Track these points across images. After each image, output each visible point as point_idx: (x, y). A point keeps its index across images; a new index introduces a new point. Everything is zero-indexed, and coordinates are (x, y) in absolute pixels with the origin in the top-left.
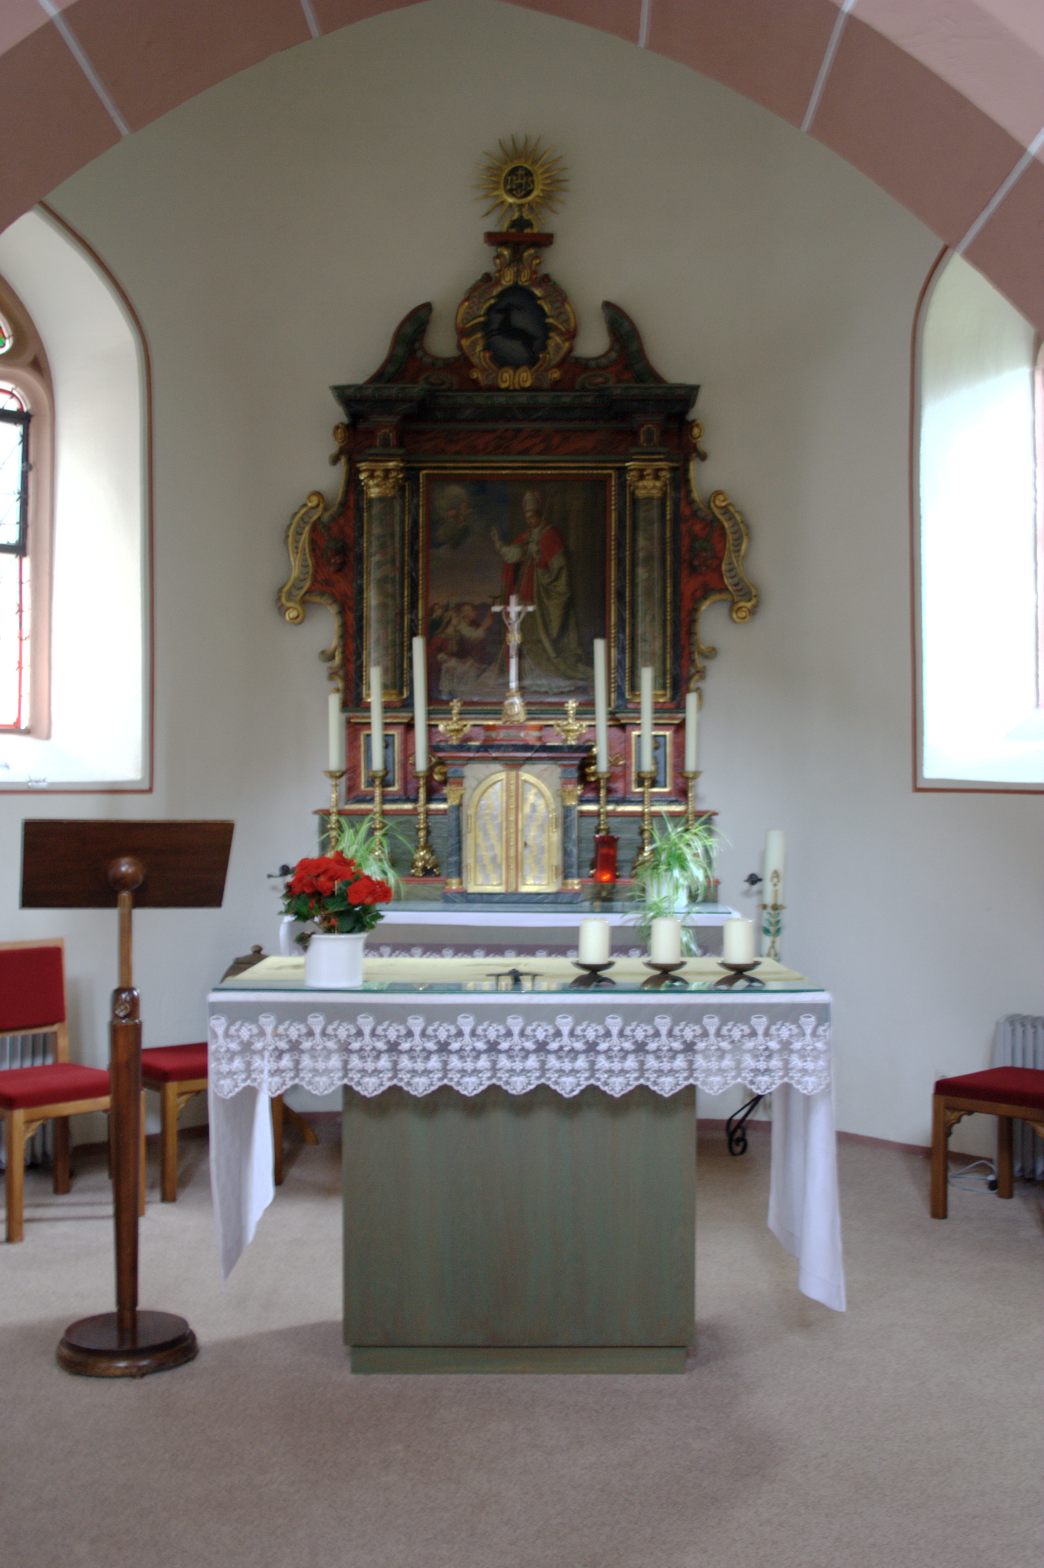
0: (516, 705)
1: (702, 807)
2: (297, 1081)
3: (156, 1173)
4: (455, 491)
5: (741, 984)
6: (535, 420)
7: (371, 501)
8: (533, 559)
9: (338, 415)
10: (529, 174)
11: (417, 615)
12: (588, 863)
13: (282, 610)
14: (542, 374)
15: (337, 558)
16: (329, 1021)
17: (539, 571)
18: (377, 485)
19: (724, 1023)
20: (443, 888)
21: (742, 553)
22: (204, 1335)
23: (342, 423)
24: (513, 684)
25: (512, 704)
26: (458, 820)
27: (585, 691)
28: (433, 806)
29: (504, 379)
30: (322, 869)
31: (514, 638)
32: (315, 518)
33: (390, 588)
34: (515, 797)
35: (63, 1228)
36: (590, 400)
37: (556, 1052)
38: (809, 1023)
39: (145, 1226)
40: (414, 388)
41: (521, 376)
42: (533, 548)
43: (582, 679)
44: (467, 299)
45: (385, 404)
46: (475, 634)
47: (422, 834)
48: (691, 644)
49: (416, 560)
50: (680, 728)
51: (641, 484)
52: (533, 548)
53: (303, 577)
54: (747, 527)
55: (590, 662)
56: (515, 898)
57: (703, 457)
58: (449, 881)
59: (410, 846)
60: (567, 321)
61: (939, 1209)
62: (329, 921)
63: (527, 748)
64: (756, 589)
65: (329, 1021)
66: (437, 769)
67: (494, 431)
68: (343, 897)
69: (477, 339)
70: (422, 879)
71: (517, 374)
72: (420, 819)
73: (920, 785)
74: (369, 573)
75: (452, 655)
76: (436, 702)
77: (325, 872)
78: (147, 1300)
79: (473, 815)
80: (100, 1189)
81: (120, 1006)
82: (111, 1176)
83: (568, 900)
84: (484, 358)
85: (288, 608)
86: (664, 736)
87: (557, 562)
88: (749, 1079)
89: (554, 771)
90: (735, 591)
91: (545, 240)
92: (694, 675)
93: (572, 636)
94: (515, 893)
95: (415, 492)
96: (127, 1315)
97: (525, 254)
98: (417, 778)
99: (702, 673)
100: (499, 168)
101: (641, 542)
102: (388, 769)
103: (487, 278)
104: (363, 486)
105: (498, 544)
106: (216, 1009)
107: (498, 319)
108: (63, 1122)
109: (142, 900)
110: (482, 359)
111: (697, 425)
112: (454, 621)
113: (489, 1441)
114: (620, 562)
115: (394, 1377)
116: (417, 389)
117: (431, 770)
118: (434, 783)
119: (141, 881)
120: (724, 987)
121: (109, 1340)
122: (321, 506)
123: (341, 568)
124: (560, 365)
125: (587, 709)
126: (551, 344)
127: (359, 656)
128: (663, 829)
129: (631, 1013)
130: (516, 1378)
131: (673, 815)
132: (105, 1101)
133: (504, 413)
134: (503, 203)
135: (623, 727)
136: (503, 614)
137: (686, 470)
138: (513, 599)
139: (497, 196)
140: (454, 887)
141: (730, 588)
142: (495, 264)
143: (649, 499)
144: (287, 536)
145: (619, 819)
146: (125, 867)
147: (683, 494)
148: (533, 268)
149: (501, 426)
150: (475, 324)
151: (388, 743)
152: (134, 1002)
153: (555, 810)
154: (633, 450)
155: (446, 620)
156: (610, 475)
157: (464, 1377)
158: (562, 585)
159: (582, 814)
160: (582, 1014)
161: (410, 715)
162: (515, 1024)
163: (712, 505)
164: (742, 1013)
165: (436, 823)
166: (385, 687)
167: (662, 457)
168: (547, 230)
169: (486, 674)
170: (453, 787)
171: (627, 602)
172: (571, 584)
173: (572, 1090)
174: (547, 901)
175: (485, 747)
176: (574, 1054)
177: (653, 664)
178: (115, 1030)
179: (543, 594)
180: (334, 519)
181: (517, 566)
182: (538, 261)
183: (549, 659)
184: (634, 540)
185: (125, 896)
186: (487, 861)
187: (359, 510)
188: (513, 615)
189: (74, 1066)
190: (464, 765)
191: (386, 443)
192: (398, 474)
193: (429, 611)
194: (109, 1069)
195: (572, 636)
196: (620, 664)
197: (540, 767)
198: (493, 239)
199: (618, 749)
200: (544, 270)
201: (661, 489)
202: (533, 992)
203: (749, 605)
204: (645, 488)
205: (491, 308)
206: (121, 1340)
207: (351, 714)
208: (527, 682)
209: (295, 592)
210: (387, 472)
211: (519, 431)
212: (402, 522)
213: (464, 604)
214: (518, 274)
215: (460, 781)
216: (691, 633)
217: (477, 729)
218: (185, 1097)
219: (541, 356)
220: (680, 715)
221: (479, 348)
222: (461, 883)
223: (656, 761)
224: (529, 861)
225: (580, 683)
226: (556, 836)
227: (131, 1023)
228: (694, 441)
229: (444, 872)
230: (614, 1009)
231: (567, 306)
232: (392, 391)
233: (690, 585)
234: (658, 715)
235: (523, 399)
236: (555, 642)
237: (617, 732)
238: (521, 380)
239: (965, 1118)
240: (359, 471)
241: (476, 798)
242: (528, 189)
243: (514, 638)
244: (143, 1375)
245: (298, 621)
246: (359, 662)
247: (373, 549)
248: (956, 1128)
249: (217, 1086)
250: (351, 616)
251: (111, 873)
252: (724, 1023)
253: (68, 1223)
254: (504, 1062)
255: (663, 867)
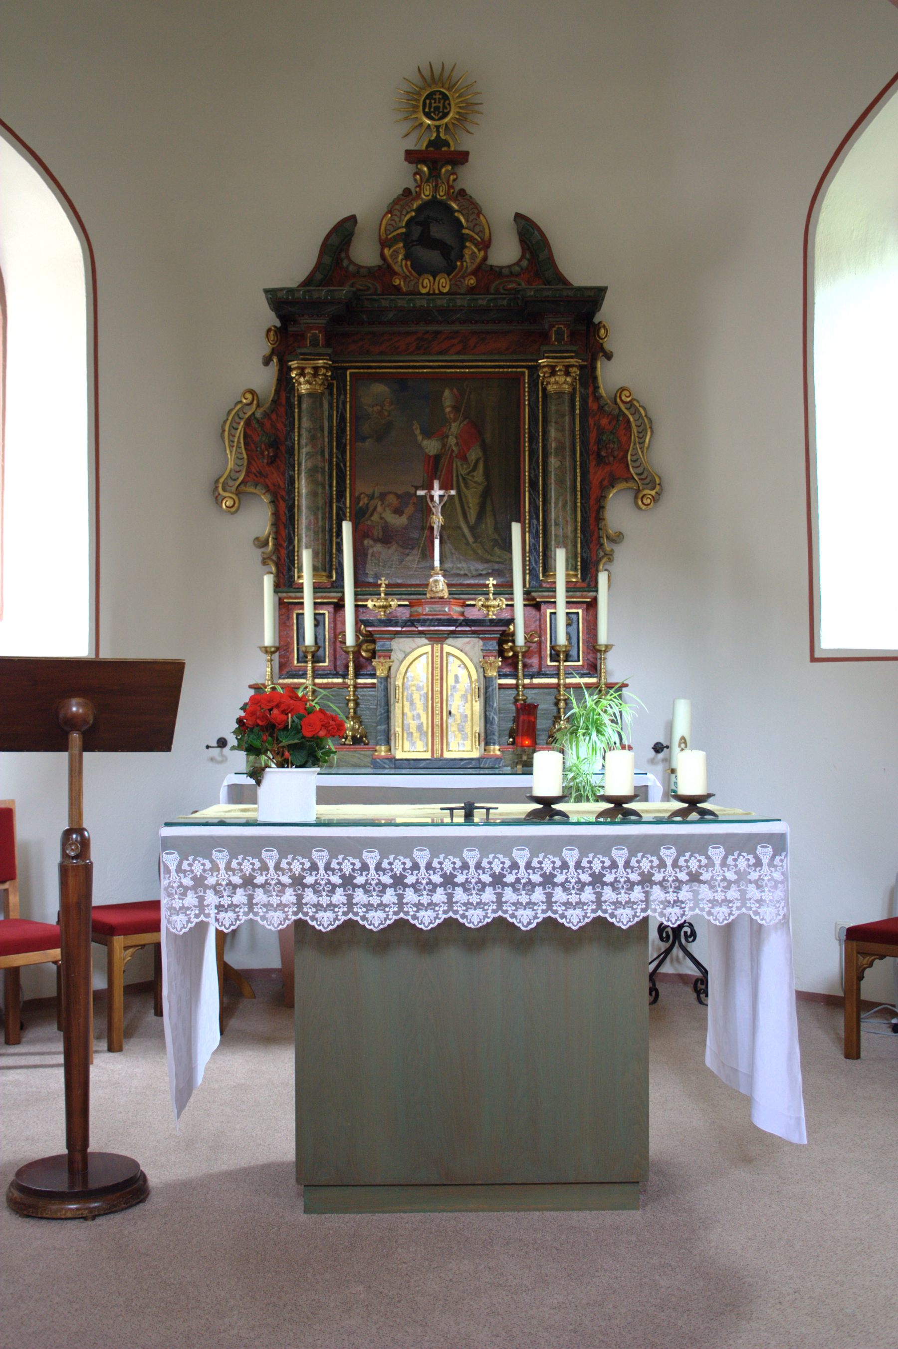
0: (440, 584)
1: (611, 680)
2: (251, 916)
3: (104, 1025)
4: (380, 388)
5: (694, 816)
6: (453, 323)
7: (300, 397)
8: (453, 451)
9: (271, 319)
10: (445, 97)
11: (345, 503)
12: (507, 732)
13: (218, 500)
14: (460, 281)
15: (271, 450)
16: (283, 855)
17: (457, 463)
18: (308, 382)
19: (680, 853)
20: (372, 755)
21: (646, 444)
22: (154, 1178)
23: (275, 327)
24: (437, 563)
25: (436, 581)
26: (386, 689)
27: (504, 572)
28: (360, 681)
29: (425, 285)
30: (275, 703)
31: (437, 520)
32: (249, 413)
33: (320, 477)
34: (438, 672)
35: (13, 1075)
36: (505, 302)
37: (512, 885)
38: (765, 853)
39: (94, 1073)
40: (343, 290)
41: (441, 281)
42: (452, 441)
43: (498, 563)
44: (390, 212)
45: (313, 306)
46: (398, 521)
47: (351, 705)
48: (599, 529)
49: (344, 453)
50: (592, 606)
51: (552, 380)
52: (452, 441)
53: (238, 469)
54: (650, 420)
55: (508, 547)
56: (440, 764)
57: (609, 356)
58: (378, 748)
59: (342, 716)
60: (483, 231)
61: (852, 1050)
62: (283, 755)
63: (451, 622)
64: (660, 478)
65: (283, 855)
66: (364, 647)
67: (415, 333)
68: (297, 730)
69: (399, 248)
70: (353, 747)
71: (437, 279)
72: (349, 691)
73: (817, 655)
74: (300, 465)
75: (377, 540)
76: (363, 587)
77: (277, 706)
78: (97, 1143)
79: (400, 685)
80: (50, 1040)
81: (71, 845)
82: (59, 1029)
83: (491, 765)
84: (406, 265)
85: (225, 498)
86: (577, 613)
87: (474, 454)
88: (707, 909)
89: (475, 645)
90: (640, 479)
91: (461, 158)
92: (603, 557)
93: (489, 522)
94: (441, 759)
95: (342, 389)
96: (78, 1157)
97: (443, 170)
98: (347, 653)
99: (610, 557)
100: (419, 94)
101: (553, 433)
102: (319, 645)
103: (407, 192)
104: (294, 383)
105: (420, 438)
106: (167, 844)
107: (417, 231)
108: (13, 973)
109: (89, 746)
110: (404, 267)
111: (604, 327)
112: (379, 509)
113: (451, 1280)
114: (533, 453)
115: (347, 1217)
116: (343, 292)
117: (359, 645)
118: (362, 659)
119: (91, 722)
120: (679, 819)
121: (60, 1182)
122: (255, 402)
123: (272, 461)
124: (475, 273)
125: (506, 589)
126: (467, 253)
127: (291, 541)
128: (580, 698)
129: (587, 845)
130: (472, 1215)
131: (588, 686)
132: (56, 953)
133: (425, 316)
134: (421, 124)
135: (537, 606)
136: (428, 497)
137: (594, 368)
138: (436, 484)
139: (417, 118)
140: (383, 754)
141: (635, 476)
142: (415, 180)
143: (560, 394)
144: (224, 431)
145: (536, 691)
146: (75, 708)
147: (591, 390)
148: (451, 183)
149: (422, 328)
150: (398, 234)
151: (318, 621)
152: (85, 844)
153: (478, 680)
154: (544, 348)
155: (371, 508)
156: (524, 373)
157: (419, 1216)
158: (479, 475)
159: (501, 687)
160: (538, 845)
161: (340, 595)
162: (471, 856)
163: (618, 400)
164: (700, 845)
165: (362, 696)
166: (315, 569)
167: (573, 354)
168: (466, 149)
169: (409, 558)
170: (382, 660)
171: (540, 491)
172: (487, 474)
173: (529, 923)
174: (471, 766)
175: (411, 622)
176: (531, 886)
177: (565, 546)
178: (64, 871)
179: (462, 484)
180: (266, 415)
181: (437, 458)
182: (455, 177)
183: (468, 544)
184: (545, 432)
185: (75, 737)
186: (413, 729)
187: (291, 406)
188: (436, 499)
189: (24, 922)
190: (391, 639)
191: (315, 343)
192: (327, 372)
193: (355, 500)
194: (58, 922)
195: (489, 522)
196: (534, 548)
197: (461, 641)
198: (411, 156)
199: (533, 627)
200: (458, 186)
201: (572, 384)
202: (487, 823)
203: (653, 493)
204: (557, 383)
205: (411, 219)
206: (72, 1183)
207: (284, 595)
208: (448, 565)
209: (231, 483)
210: (316, 369)
211: (438, 333)
212: (330, 417)
213: (390, 493)
214: (436, 189)
215: (388, 654)
216: (599, 519)
217: (401, 609)
218: (131, 950)
219: (459, 264)
220: (592, 594)
221: (400, 257)
222: (390, 750)
223: (569, 636)
224: (453, 728)
225: (496, 566)
226: (478, 706)
227: (81, 863)
228: (601, 341)
229: (372, 742)
230: (571, 841)
231: (482, 217)
232: (322, 293)
233: (597, 475)
234: (571, 594)
235: (442, 302)
236: (472, 529)
237: (533, 611)
238: (440, 286)
239: (877, 962)
240: (290, 369)
241: (403, 669)
242: (445, 111)
243: (437, 520)
244: (94, 1218)
245: (233, 510)
246: (291, 548)
247: (304, 441)
248: (867, 972)
249: (169, 922)
250: (282, 505)
251: (61, 715)
252: (680, 853)
253: (18, 1071)
254: (459, 895)
255: (581, 731)
